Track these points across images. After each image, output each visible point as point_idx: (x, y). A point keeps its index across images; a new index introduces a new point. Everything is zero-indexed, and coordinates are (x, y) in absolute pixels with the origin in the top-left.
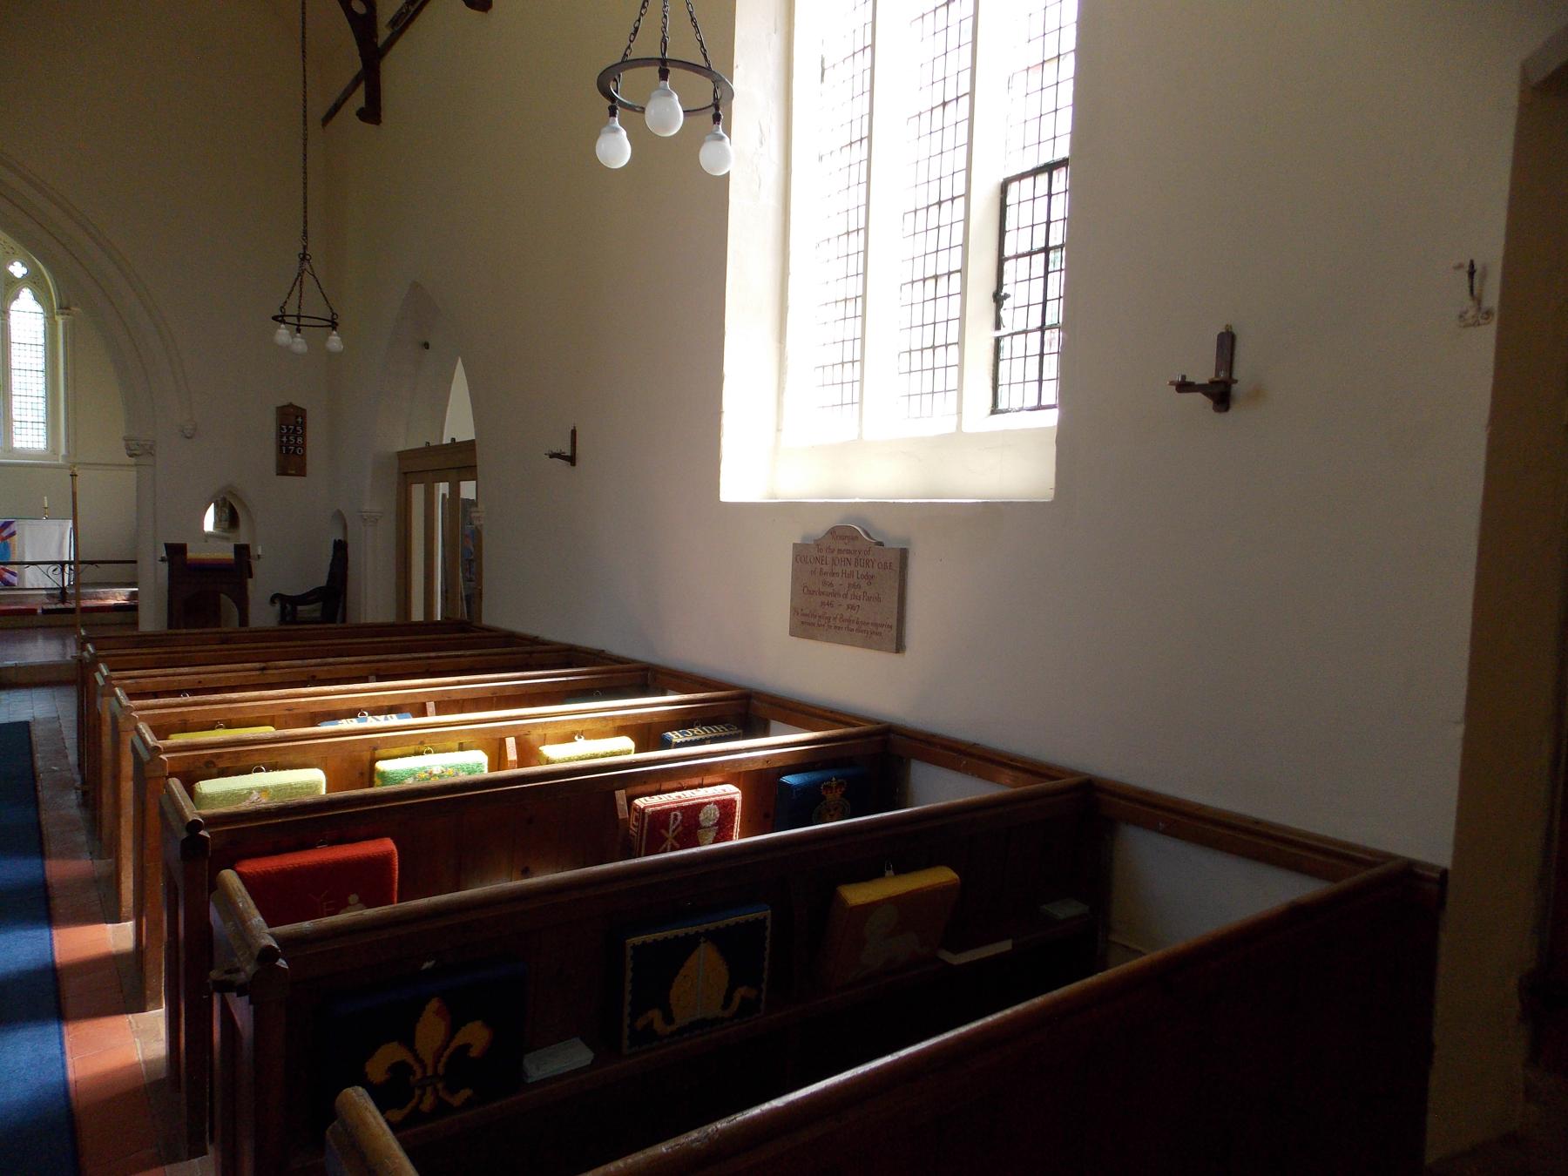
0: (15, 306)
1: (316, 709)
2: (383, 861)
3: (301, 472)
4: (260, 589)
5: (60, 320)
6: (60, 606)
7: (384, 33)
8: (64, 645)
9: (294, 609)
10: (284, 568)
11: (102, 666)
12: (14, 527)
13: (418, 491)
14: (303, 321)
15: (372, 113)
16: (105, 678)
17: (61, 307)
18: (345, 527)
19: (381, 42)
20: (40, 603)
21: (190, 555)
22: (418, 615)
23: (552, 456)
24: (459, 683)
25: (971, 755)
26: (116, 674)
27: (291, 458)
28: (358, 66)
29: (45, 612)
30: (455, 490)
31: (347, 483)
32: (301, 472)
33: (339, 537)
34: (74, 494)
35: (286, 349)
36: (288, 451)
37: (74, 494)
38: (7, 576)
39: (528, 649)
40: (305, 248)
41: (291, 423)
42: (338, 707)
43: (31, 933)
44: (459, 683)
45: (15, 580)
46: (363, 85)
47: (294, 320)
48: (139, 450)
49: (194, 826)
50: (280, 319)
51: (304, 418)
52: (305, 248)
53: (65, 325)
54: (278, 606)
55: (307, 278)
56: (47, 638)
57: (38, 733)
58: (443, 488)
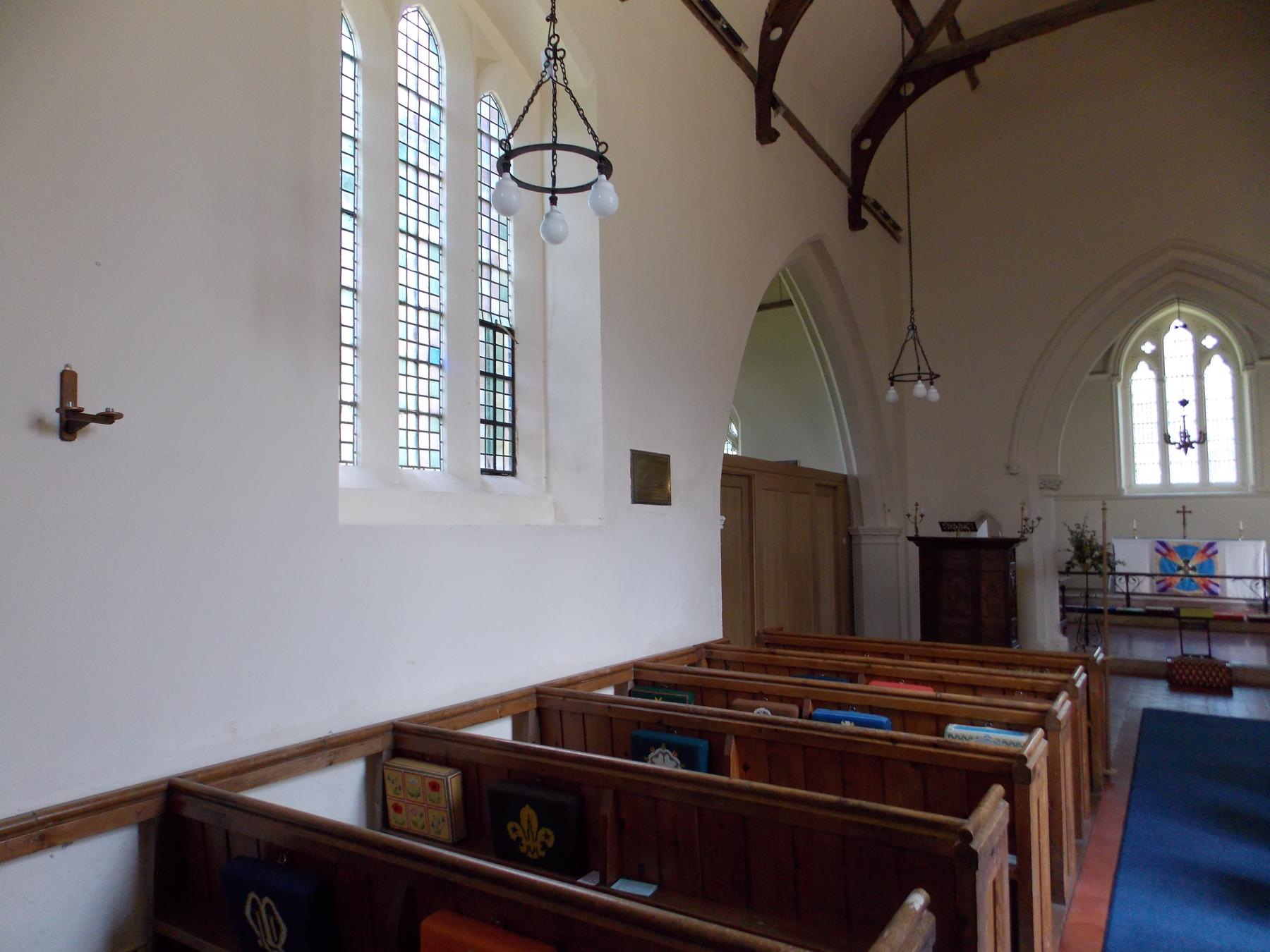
0: (1135, 376)
5: (1246, 376)
6: (1263, 616)
12: (1218, 547)
17: (1246, 364)
20: (1246, 613)
25: (455, 715)
29: (1252, 620)
35: (924, 400)
38: (1212, 586)
45: (1218, 590)
53: (1250, 379)
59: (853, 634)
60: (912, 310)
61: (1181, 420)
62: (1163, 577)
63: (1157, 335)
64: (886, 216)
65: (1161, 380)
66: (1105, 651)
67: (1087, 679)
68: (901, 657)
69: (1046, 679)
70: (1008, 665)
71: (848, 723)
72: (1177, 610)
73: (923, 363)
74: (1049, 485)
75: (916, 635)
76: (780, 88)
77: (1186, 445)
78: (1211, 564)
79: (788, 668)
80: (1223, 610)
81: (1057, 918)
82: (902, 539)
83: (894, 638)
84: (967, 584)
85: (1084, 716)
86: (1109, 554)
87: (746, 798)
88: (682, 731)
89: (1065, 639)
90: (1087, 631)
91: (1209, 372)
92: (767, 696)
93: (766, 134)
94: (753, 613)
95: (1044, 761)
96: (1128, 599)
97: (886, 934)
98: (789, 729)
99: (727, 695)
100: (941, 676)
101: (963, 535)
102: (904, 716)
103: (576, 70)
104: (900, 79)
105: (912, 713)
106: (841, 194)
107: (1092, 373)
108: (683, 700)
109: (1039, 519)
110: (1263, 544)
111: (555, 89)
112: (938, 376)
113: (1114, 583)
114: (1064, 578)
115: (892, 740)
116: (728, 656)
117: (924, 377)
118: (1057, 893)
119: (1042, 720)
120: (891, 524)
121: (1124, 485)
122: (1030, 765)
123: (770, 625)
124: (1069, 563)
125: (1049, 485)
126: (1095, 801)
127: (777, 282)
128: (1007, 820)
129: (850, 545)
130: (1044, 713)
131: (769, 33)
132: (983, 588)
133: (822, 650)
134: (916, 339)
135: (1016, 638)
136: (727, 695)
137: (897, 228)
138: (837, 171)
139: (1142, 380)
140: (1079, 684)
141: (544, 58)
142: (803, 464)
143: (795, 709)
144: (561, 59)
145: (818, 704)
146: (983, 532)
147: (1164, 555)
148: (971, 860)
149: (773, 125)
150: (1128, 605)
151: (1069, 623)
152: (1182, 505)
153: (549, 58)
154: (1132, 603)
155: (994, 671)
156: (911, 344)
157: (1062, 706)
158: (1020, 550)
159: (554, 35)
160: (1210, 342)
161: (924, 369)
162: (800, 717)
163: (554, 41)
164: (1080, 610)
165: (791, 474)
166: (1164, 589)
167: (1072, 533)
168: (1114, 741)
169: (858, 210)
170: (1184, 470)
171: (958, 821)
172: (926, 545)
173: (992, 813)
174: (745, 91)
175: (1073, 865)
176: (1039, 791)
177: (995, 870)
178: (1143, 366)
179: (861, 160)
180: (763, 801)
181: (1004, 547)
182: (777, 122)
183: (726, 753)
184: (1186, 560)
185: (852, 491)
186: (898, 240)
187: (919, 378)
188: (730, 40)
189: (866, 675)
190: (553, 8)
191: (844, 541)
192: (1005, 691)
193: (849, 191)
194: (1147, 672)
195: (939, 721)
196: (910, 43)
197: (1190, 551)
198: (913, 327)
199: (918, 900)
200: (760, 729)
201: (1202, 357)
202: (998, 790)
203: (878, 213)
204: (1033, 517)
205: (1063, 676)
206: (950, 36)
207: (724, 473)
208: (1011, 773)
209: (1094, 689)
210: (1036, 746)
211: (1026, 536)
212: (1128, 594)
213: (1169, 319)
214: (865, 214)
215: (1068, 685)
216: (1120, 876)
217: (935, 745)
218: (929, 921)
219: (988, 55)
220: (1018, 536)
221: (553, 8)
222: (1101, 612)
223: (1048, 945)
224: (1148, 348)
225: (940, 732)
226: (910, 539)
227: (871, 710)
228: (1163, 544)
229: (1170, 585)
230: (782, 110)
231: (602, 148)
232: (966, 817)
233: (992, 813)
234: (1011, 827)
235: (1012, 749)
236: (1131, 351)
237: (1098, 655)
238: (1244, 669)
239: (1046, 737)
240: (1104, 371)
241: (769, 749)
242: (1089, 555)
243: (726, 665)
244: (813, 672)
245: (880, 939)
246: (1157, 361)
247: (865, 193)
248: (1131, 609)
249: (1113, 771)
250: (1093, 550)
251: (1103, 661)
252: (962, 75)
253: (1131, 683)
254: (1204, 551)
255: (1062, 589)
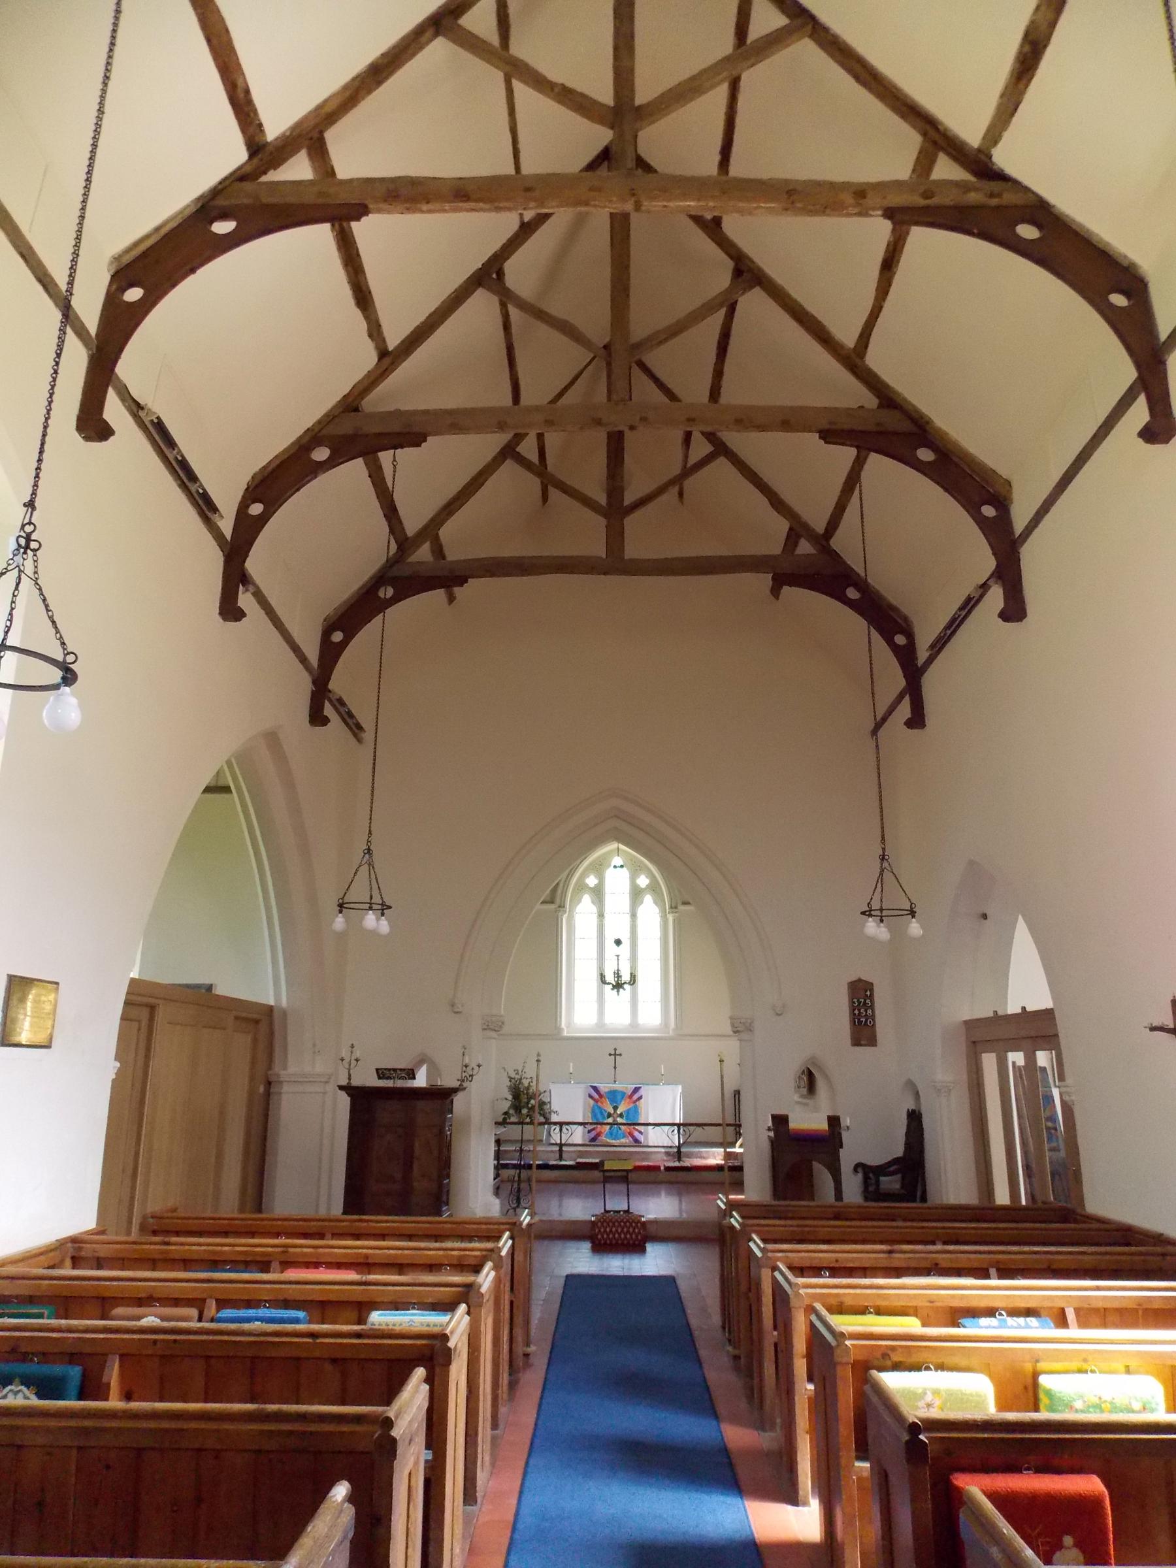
1: (956, 1304)
2: (1085, 1506)
3: (872, 1041)
4: (848, 1157)
5: (670, 918)
6: (677, 1164)
7: (922, 655)
8: (680, 1201)
9: (878, 1182)
10: (870, 1142)
11: (754, 1236)
12: (642, 1092)
13: (989, 1061)
14: (884, 913)
15: (917, 720)
16: (762, 1250)
17: (671, 907)
18: (917, 1095)
19: (921, 661)
21: (793, 1125)
22: (1002, 1197)
23: (1153, 1029)
24: (1098, 1288)
26: (770, 1246)
27: (863, 1029)
28: (902, 683)
29: (668, 1169)
30: (1031, 1059)
31: (917, 1058)
32: (872, 1041)
33: (912, 1106)
34: (722, 1077)
35: (374, 933)
36: (860, 1022)
37: (722, 1077)
38: (636, 1134)
39: (1159, 1249)
40: (884, 849)
41: (861, 996)
42: (974, 1304)
43: (722, 1498)
44: (1098, 1288)
45: (641, 1138)
46: (907, 698)
47: (878, 913)
48: (741, 1028)
49: (914, 1429)
50: (868, 913)
51: (872, 990)
52: (884, 849)
53: (674, 921)
54: (860, 1175)
55: (887, 875)
56: (668, 1194)
57: (683, 1285)
58: (1016, 1058)
59: (260, 1211)
60: (370, 833)
61: (617, 961)
62: (593, 1126)
63: (599, 868)
64: (350, 715)
65: (601, 915)
66: (532, 1214)
67: (513, 1246)
68: (321, 1236)
69: (472, 1250)
70: (437, 1238)
71: (258, 1323)
72: (602, 1163)
73: (375, 893)
74: (493, 1026)
75: (337, 1209)
76: (254, 564)
77: (618, 986)
78: (636, 1111)
79: (184, 1261)
80: (643, 1160)
81: (467, 1520)
82: (331, 1088)
83: (309, 1213)
84: (397, 1141)
85: (508, 1288)
86: (544, 1103)
87: (144, 1424)
88: (45, 1357)
89: (497, 1201)
90: (519, 1190)
91: (641, 911)
92: (159, 1300)
93: (230, 611)
94: (133, 1188)
95: (465, 1339)
96: (561, 1151)
97: (309, 1529)
98: (192, 1337)
99: (104, 1303)
100: (367, 1256)
101: (400, 1084)
102: (323, 1308)
103: (51, 561)
104: (380, 579)
105: (330, 1302)
106: (305, 685)
107: (543, 903)
108: (40, 1316)
109: (479, 1066)
110: (680, 1088)
111: (19, 577)
112: (389, 907)
113: (549, 1134)
114: (501, 1130)
115: (313, 1335)
116: (103, 1251)
117: (375, 907)
118: (470, 1496)
119: (467, 1294)
120: (319, 1068)
121: (563, 1025)
122: (451, 1344)
123: (155, 1205)
124: (506, 1113)
125: (493, 1026)
126: (513, 1385)
127: (218, 774)
128: (426, 1405)
129: (268, 1094)
130: (469, 1286)
131: (248, 507)
132: (417, 1145)
133: (226, 1234)
134: (371, 864)
135: (447, 1204)
136: (104, 1303)
137: (359, 727)
138: (303, 660)
139: (583, 913)
140: (503, 1253)
141: (14, 546)
142: (220, 990)
143: (194, 1312)
144: (34, 550)
145: (222, 1304)
146: (421, 1080)
147: (596, 1101)
148: (389, 1447)
149: (240, 604)
150: (561, 1158)
151: (502, 1181)
152: (615, 1050)
153: (19, 545)
154: (564, 1156)
155: (422, 1245)
156: (365, 868)
157: (486, 1279)
158: (458, 1100)
159: (30, 523)
160: (643, 881)
161: (377, 899)
162: (200, 1320)
163: (28, 529)
164: (515, 1166)
165: (201, 1000)
166: (593, 1139)
167: (511, 1079)
168: (536, 1314)
169: (321, 704)
170: (617, 1013)
171: (380, 1409)
172: (361, 1098)
173: (412, 1397)
174: (213, 561)
175: (487, 1458)
176: (458, 1372)
177: (412, 1460)
178: (586, 899)
179: (330, 653)
180: (165, 1425)
181: (441, 1097)
182: (245, 600)
183: (105, 1380)
184: (613, 1109)
185: (277, 1027)
186: (359, 740)
187: (371, 908)
188: (205, 506)
189: (281, 1263)
190: (34, 493)
191: (262, 1089)
192: (432, 1267)
193: (314, 682)
194: (571, 1233)
195: (362, 1308)
196: (394, 547)
197: (619, 1097)
198: (369, 851)
199: (341, 1491)
200: (155, 1342)
201: (636, 895)
202: (420, 1372)
203: (342, 709)
204: (473, 1065)
205: (489, 1245)
206: (433, 552)
207: (127, 1003)
208: (432, 1354)
209: (519, 1257)
210: (459, 1322)
211: (465, 1084)
212: (561, 1145)
213: (610, 853)
214: (328, 711)
215: (492, 1254)
216: (531, 1462)
217: (358, 1335)
218: (350, 1511)
219: (466, 582)
220: (456, 1084)
221: (34, 493)
222: (530, 1167)
223: (457, 1550)
224: (592, 881)
225: (362, 1320)
226: (341, 1088)
227: (287, 1304)
228: (595, 1088)
229: (599, 1134)
230: (251, 588)
231: (70, 659)
232: (388, 1402)
233: (414, 1396)
234: (430, 1411)
235: (436, 1330)
236: (576, 884)
237: (525, 1219)
238: (655, 1222)
239: (468, 1313)
240: (552, 902)
241: (163, 1364)
242: (525, 1105)
243: (99, 1263)
244: (215, 1264)
245: (304, 1534)
246: (598, 894)
247: (330, 686)
248: (563, 1163)
249: (532, 1349)
250: (529, 1099)
251: (529, 1225)
252: (439, 594)
253: (558, 1246)
254: (631, 1096)
255: (498, 1142)
